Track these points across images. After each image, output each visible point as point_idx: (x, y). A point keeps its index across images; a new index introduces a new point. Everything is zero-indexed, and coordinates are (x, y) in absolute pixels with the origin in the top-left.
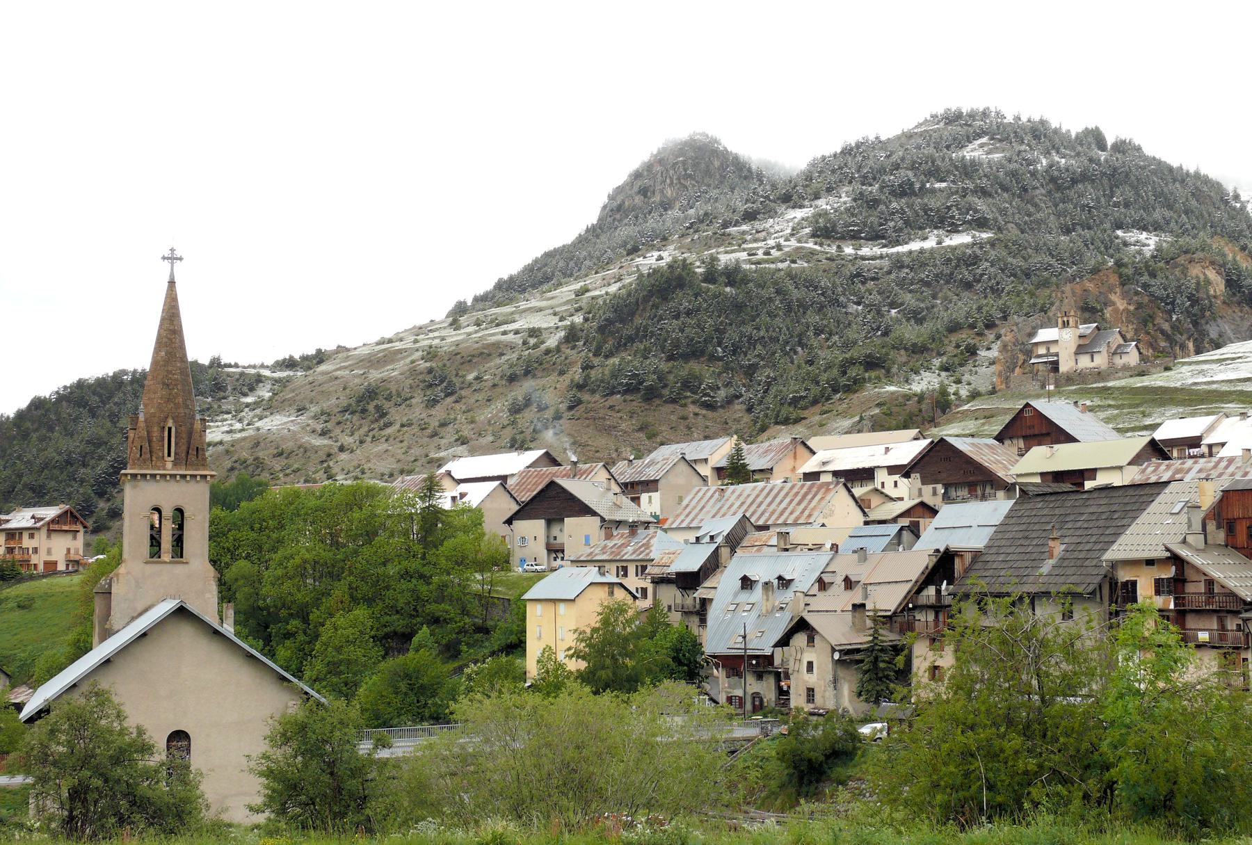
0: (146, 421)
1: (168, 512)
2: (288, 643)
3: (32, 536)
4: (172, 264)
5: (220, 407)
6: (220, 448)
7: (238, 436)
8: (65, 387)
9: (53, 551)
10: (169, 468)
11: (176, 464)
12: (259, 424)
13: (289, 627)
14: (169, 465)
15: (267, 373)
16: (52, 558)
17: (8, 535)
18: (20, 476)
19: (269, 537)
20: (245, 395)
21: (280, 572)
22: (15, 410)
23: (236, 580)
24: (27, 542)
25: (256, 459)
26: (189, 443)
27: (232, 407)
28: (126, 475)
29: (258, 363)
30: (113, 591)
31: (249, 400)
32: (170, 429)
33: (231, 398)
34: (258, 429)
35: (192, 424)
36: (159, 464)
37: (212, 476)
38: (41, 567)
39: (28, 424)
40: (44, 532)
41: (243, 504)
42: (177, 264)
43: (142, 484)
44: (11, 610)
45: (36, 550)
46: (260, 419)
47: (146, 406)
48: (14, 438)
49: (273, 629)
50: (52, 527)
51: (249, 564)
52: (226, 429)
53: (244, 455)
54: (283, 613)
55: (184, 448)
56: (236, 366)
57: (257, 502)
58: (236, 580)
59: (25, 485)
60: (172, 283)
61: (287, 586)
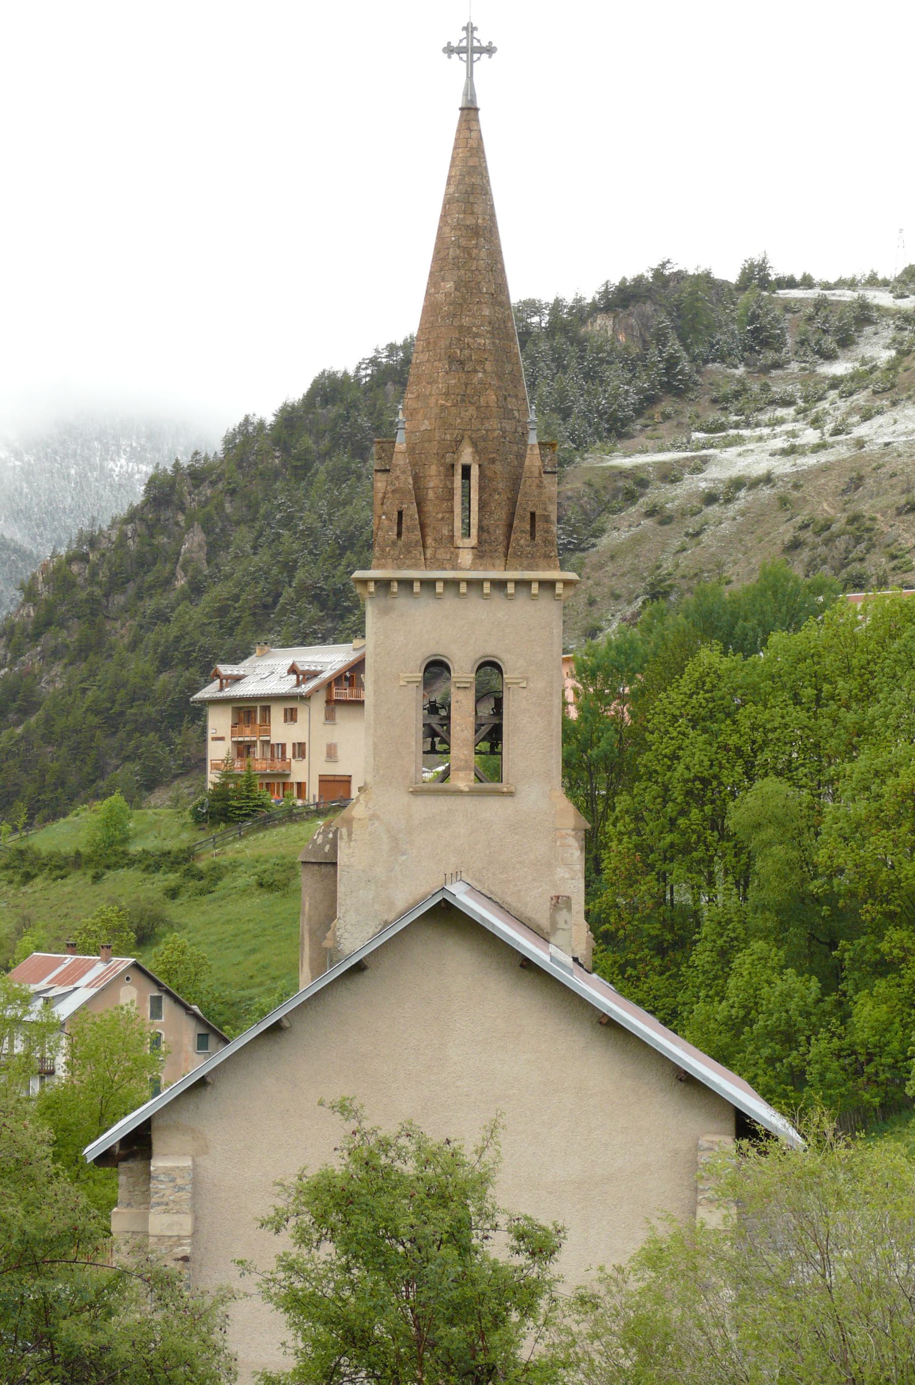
0: (411, 450)
1: (463, 671)
2: (881, 986)
3: (291, 716)
4: (470, 64)
5: (765, 388)
6: (766, 492)
7: (811, 460)
8: (392, 348)
9: (340, 753)
10: (466, 565)
11: (481, 553)
12: (862, 430)
13: (884, 946)
14: (466, 558)
15: (883, 298)
16: (338, 770)
17: (237, 711)
18: (290, 568)
19: (836, 722)
20: (829, 357)
21: (861, 808)
22: (276, 406)
23: (758, 826)
24: (281, 731)
25: (854, 519)
26: (513, 502)
27: (794, 389)
28: (364, 582)
29: (861, 272)
30: (342, 859)
31: (840, 368)
32: (466, 471)
33: (794, 367)
34: (860, 444)
35: (521, 457)
36: (442, 554)
37: (567, 583)
38: (313, 791)
39: (308, 441)
40: (318, 706)
41: (775, 638)
42: (483, 63)
43: (402, 603)
44: (245, 892)
45: (300, 750)
46: (867, 417)
47: (411, 414)
48: (277, 475)
49: (847, 951)
50: (339, 693)
51: (784, 787)
52: (780, 443)
53: (826, 508)
54: (869, 912)
55: (500, 515)
56: (807, 282)
57: (812, 633)
58: (758, 826)
59: (303, 589)
60: (469, 111)
61: (879, 843)
